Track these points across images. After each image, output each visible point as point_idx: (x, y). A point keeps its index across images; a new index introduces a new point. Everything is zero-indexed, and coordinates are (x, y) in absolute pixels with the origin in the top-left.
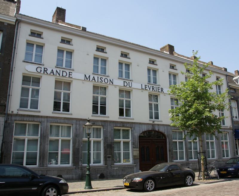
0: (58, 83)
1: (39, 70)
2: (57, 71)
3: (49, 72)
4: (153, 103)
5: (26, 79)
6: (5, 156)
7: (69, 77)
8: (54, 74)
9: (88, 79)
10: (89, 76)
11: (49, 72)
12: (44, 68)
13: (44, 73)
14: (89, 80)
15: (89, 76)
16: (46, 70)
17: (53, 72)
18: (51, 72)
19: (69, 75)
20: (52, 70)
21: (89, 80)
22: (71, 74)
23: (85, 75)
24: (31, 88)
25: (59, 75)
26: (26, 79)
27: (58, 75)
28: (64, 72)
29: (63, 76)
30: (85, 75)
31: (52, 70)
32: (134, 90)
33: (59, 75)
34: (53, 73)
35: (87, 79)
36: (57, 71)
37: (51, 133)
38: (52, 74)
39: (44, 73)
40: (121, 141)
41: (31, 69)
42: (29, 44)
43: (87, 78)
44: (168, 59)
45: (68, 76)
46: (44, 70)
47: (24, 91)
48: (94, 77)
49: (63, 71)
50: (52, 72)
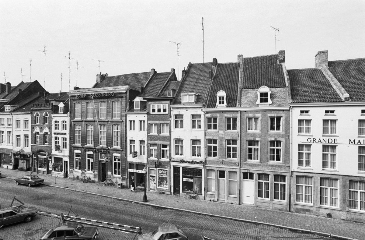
0: (325, 147)
1: (309, 140)
2: (323, 139)
3: (317, 141)
4: (57, 141)
5: (300, 146)
6: (291, 127)
7: (334, 143)
8: (321, 142)
9: (353, 143)
10: (354, 140)
11: (317, 141)
12: (313, 139)
13: (313, 142)
14: (355, 143)
15: (354, 140)
16: (314, 139)
17: (360, 141)
18: (358, 142)
19: (335, 141)
20: (320, 139)
21: (355, 143)
22: (335, 140)
23: (350, 140)
24: (329, 153)
25: (326, 142)
26: (300, 146)
27: (324, 142)
28: (329, 140)
29: (329, 143)
30: (350, 140)
31: (320, 139)
32: (338, 145)
33: (326, 142)
34: (320, 141)
35: (352, 143)
36: (323, 139)
37: (76, 167)
38: (320, 142)
39: (313, 142)
40: (180, 167)
41: (303, 140)
42: (300, 121)
43: (352, 142)
44: (226, 112)
45: (333, 142)
46: (313, 140)
47: (300, 155)
48: (359, 141)
49: (329, 139)
50: (320, 141)
